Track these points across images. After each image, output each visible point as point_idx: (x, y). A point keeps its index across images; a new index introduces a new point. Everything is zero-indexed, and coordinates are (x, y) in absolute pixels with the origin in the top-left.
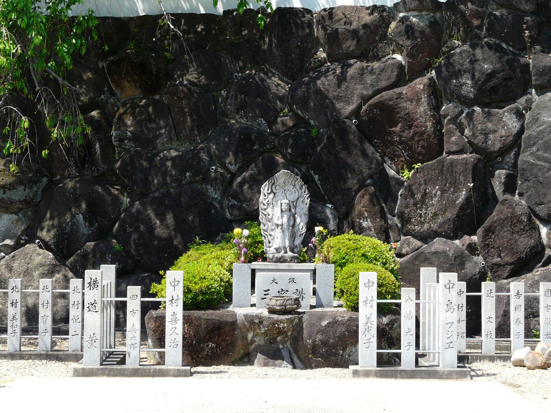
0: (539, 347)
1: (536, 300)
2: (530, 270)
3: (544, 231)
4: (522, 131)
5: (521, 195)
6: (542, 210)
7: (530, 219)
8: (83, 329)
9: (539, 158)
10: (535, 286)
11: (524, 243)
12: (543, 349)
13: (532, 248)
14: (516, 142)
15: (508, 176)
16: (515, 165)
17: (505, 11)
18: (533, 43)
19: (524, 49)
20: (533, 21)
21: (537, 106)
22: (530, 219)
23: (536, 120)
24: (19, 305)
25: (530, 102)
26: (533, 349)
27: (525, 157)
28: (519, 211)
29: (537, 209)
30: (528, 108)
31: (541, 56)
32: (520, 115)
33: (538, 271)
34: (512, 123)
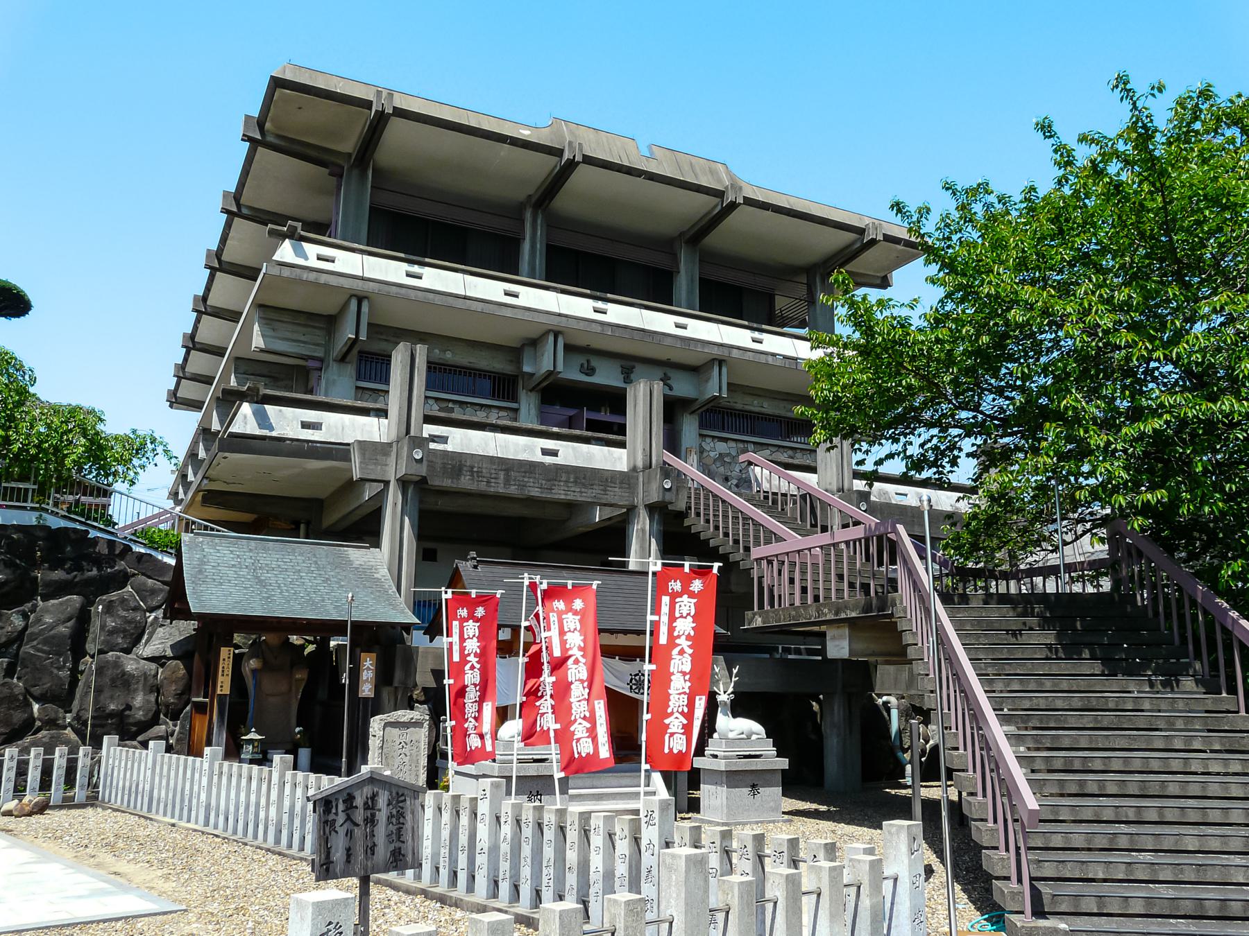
0: (26, 800)
1: (27, 762)
2: (21, 739)
3: (36, 707)
4: (26, 628)
5: (19, 678)
6: (36, 691)
7: (25, 698)
8: (80, 897)
9: (39, 650)
10: (26, 750)
11: (18, 717)
12: (30, 801)
13: (25, 721)
14: (20, 637)
15: (9, 664)
16: (17, 654)
17: (21, 536)
18: (43, 561)
19: (35, 565)
20: (112, 697)
21: (42, 610)
22: (25, 698)
23: (39, 621)
24: (785, 854)
25: (35, 606)
26: (21, 801)
27: (27, 649)
28: (16, 691)
29: (32, 690)
30: (33, 610)
31: (48, 572)
32: (25, 616)
33: (28, 739)
34: (17, 622)
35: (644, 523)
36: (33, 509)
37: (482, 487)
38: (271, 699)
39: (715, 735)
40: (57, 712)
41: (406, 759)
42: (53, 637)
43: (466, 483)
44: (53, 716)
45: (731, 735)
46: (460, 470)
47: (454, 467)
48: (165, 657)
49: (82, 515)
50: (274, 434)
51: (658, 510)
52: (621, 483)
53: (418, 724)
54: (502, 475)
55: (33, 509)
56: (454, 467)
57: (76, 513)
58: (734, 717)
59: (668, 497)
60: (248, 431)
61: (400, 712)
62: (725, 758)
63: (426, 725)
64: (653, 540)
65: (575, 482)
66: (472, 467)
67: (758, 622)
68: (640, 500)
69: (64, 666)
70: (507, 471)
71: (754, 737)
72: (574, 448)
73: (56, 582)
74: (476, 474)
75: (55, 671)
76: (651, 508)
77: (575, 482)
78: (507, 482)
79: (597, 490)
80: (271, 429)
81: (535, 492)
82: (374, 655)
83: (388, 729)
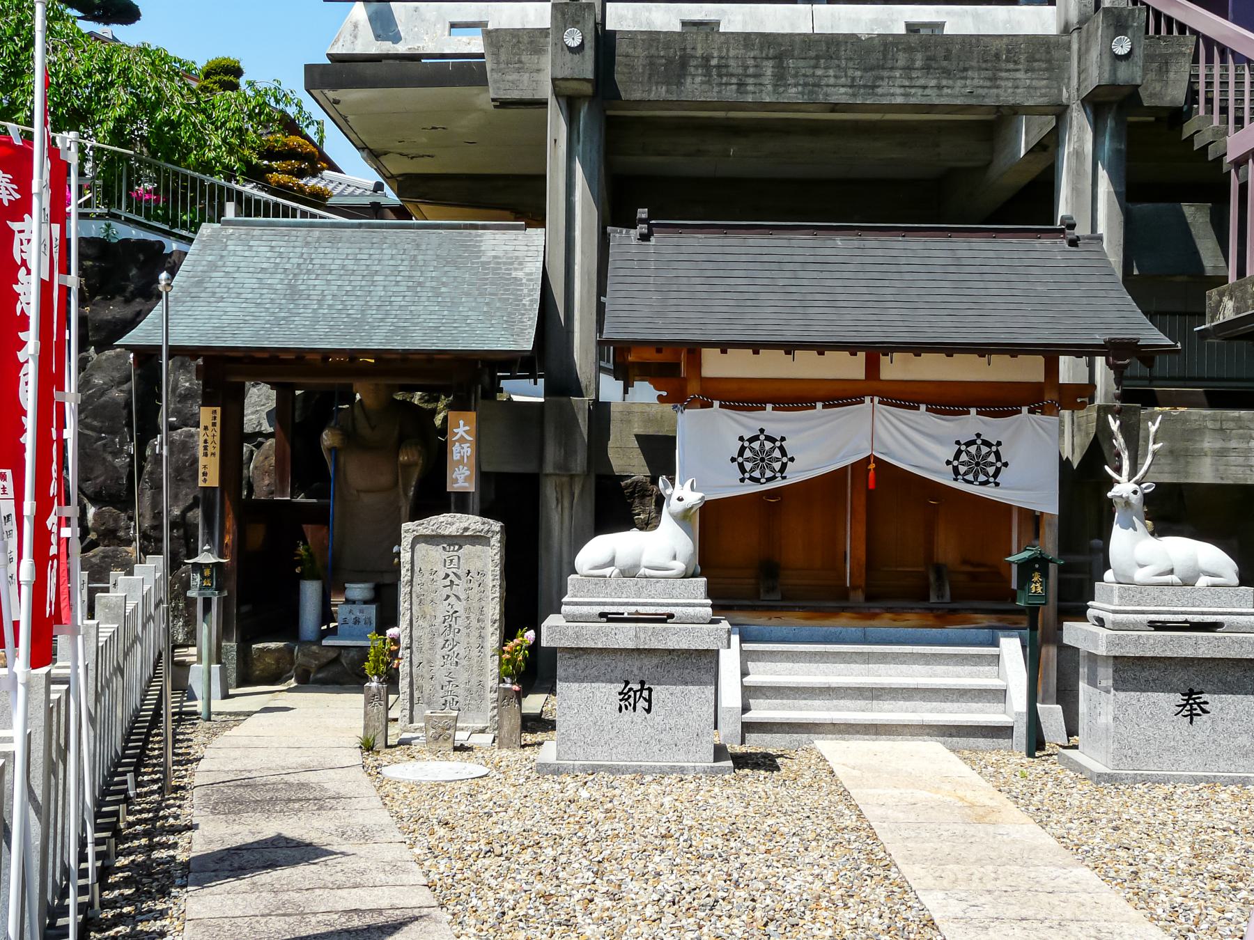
35: (1081, 139)
36: (100, 217)
37: (730, 94)
38: (367, 499)
39: (1109, 575)
40: (116, 520)
41: (459, 606)
42: (104, 406)
43: (695, 88)
44: (111, 524)
45: (1140, 575)
46: (684, 62)
47: (670, 61)
48: (260, 434)
49: (165, 220)
50: (401, 48)
51: (1109, 104)
52: (1031, 59)
53: (479, 539)
54: (769, 69)
55: (100, 217)
56: (670, 61)
57: (157, 218)
58: (1158, 532)
59: (1125, 74)
60: (359, 49)
61: (443, 518)
62: (1118, 626)
63: (495, 541)
64: (1103, 175)
65: (927, 68)
66: (707, 59)
67: (1228, 311)
68: (1071, 94)
69: (121, 451)
70: (779, 58)
71: (1203, 581)
72: (976, 16)
73: (108, 322)
74: (714, 70)
75: (110, 458)
76: (1100, 104)
77: (927, 68)
78: (780, 79)
79: (975, 80)
80: (397, 39)
81: (840, 95)
82: (472, 415)
83: (421, 548)
